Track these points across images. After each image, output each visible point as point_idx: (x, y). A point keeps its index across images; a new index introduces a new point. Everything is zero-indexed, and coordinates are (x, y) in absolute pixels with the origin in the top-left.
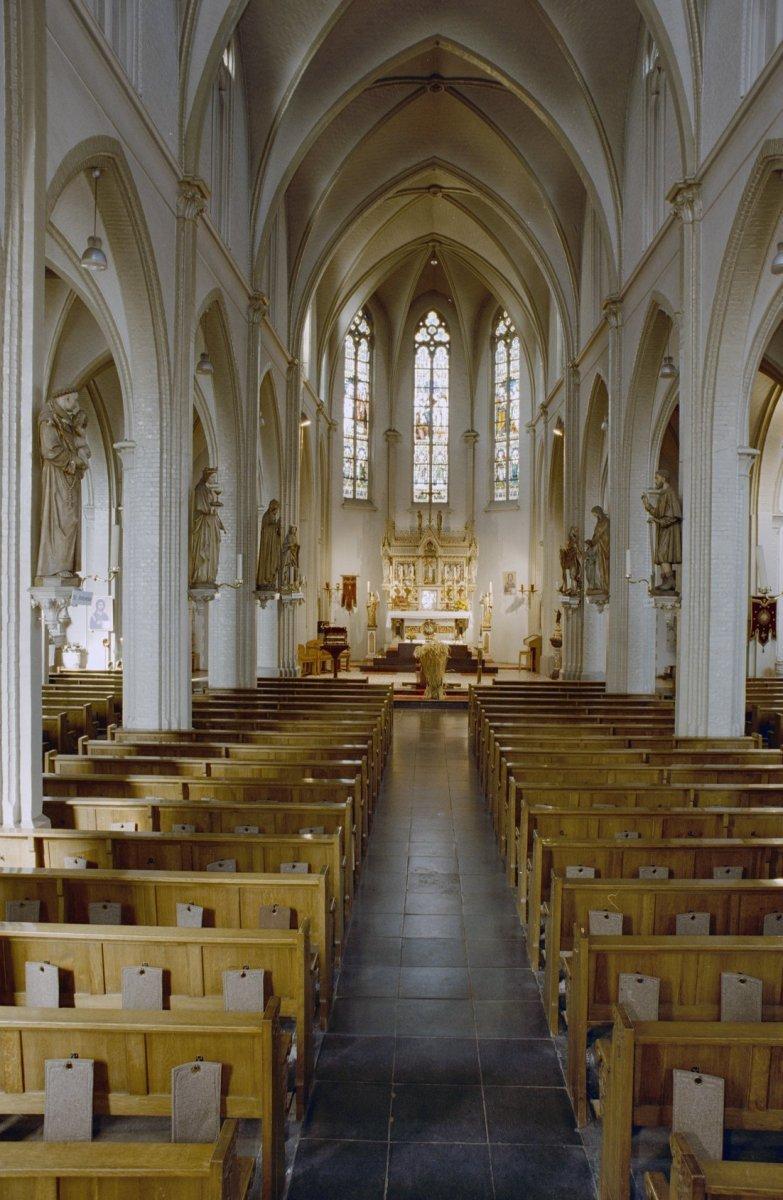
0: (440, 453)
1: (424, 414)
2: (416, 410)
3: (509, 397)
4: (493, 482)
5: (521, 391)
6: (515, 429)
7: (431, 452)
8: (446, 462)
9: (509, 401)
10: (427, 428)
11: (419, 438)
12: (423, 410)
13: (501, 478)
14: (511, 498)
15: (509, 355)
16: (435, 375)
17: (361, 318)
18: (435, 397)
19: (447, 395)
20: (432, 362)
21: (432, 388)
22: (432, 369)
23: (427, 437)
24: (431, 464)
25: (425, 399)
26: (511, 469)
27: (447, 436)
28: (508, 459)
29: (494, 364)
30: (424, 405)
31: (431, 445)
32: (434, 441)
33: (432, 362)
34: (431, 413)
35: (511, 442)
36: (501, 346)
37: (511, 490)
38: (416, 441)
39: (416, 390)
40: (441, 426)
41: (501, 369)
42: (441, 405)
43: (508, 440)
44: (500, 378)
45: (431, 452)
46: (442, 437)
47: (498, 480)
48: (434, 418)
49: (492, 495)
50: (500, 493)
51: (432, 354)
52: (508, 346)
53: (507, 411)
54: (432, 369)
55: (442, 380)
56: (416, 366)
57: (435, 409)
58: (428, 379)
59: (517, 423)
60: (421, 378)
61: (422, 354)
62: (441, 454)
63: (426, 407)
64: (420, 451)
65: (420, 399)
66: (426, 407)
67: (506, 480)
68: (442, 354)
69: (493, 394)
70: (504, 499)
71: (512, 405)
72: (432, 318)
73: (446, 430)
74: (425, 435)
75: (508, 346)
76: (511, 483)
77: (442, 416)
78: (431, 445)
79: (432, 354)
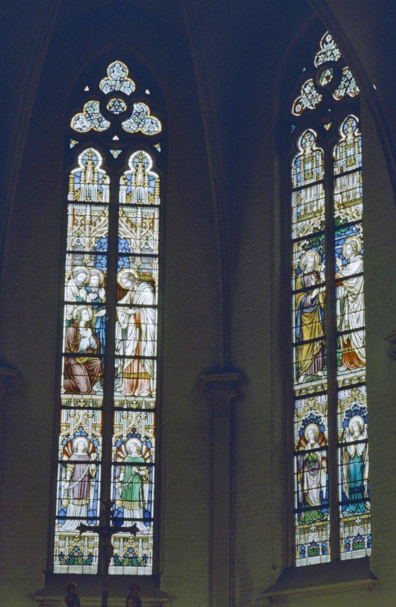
0: (133, 434)
1: (89, 325)
2: (69, 312)
3: (331, 269)
4: (290, 510)
5: (368, 253)
6: (352, 357)
7: (107, 428)
8: (154, 247)
9: (333, 283)
10: (97, 362)
11: (75, 390)
12: (86, 314)
13: (314, 498)
14: (345, 556)
15: (329, 162)
16: (122, 221)
17: (315, 74)
18: (122, 279)
19: (156, 275)
20: (114, 189)
21: (112, 254)
22: (114, 207)
23: (97, 387)
24: (106, 463)
25: (94, 281)
26: (342, 472)
27: (154, 385)
28: (333, 443)
29: (287, 189)
30: (91, 298)
31: (108, 409)
32: (118, 398)
33: (114, 189)
34: (110, 321)
35: (343, 395)
36: (307, 145)
37: (344, 532)
38: (65, 398)
39: (69, 257)
40: (138, 357)
41: (309, 203)
42: (138, 300)
43: (333, 390)
44: (302, 227)
45: (107, 428)
46: (139, 387)
47: (305, 506)
48: (118, 335)
49: (290, 549)
50: (311, 544)
51: (115, 169)
52: (328, 141)
53: (329, 311)
54: (114, 207)
55: (142, 234)
56: (70, 197)
57: (122, 313)
58: (103, 228)
59: (358, 340)
60: (84, 229)
61: (88, 174)
62: (136, 434)
63: (96, 305)
64: (78, 428)
65: (80, 281)
66: (96, 305)
67: (331, 503)
68: (142, 179)
69: (287, 270)
70: (326, 559)
71: (341, 292)
72: (117, 77)
73: (150, 367)
74: (92, 382)
75: (328, 141)
76: (345, 514)
77: (140, 331)
78: (108, 409)
79: (115, 169)
